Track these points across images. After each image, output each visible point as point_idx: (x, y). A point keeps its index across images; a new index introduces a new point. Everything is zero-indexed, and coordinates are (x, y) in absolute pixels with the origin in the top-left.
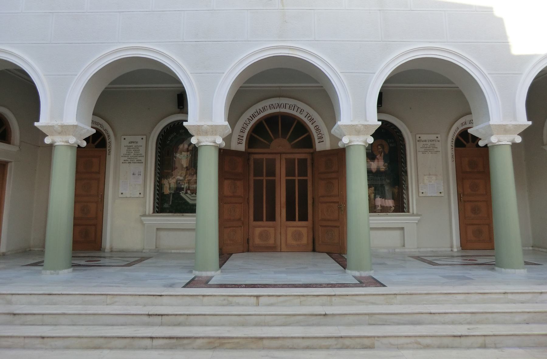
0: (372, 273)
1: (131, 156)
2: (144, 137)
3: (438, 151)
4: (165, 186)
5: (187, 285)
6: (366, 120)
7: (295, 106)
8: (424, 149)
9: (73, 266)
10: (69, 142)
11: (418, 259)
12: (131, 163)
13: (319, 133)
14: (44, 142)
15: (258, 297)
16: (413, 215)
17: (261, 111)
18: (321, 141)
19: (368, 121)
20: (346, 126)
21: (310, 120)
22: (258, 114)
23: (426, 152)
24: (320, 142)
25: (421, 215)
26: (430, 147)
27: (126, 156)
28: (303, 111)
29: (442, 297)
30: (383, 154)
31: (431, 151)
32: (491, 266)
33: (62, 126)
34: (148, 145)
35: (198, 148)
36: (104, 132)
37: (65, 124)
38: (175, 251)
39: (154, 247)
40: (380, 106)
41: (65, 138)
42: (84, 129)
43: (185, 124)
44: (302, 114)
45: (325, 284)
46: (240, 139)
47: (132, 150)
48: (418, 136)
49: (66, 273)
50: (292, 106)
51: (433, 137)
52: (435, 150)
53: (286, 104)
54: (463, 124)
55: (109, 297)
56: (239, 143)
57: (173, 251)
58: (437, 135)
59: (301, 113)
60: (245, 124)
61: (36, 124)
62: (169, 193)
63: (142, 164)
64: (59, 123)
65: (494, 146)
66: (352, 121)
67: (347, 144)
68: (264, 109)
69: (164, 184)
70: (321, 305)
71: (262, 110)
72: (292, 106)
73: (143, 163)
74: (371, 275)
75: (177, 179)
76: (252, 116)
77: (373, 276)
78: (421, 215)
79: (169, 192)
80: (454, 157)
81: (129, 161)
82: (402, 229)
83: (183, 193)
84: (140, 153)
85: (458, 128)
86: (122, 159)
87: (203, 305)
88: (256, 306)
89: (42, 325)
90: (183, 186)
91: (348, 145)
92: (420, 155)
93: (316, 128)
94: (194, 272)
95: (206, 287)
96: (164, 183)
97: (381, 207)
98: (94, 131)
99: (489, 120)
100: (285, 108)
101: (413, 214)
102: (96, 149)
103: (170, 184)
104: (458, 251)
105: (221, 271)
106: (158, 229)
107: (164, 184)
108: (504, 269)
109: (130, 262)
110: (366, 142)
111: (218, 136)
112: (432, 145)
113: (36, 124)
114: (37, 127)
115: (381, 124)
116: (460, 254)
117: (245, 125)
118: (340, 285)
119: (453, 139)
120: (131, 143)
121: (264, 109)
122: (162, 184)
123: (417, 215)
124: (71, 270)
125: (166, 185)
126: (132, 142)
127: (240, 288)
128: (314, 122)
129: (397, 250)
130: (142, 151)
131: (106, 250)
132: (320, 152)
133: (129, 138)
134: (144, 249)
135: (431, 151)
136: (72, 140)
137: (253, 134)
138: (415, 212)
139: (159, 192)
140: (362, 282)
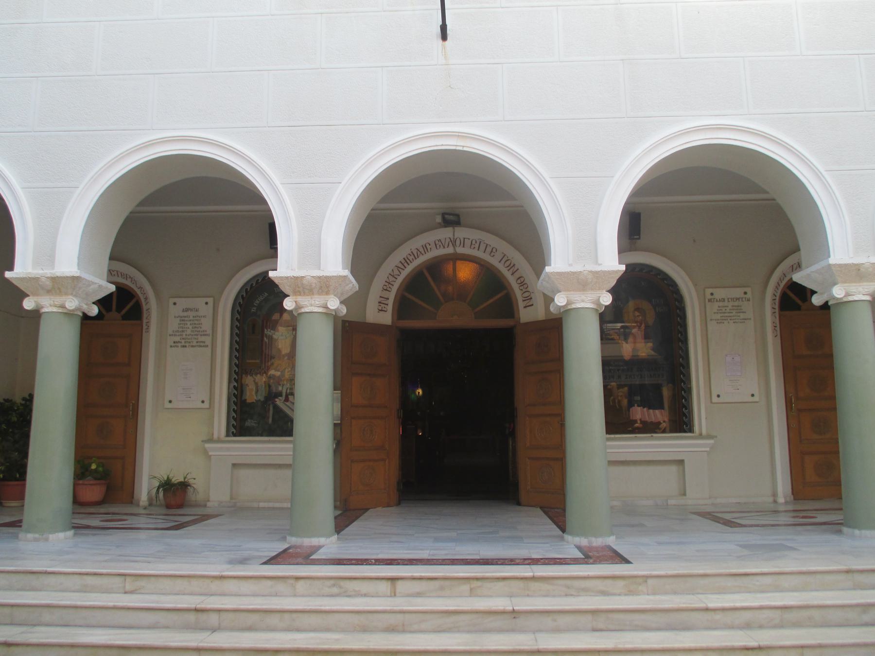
0: (611, 541)
1: (186, 335)
2: (210, 301)
3: (748, 319)
4: (248, 388)
5: (272, 561)
6: (596, 262)
7: (480, 242)
8: (722, 315)
9: (74, 528)
10: (65, 308)
11: (708, 516)
12: (186, 346)
13: (524, 290)
14: (22, 307)
15: (393, 580)
16: (701, 436)
17: (420, 252)
18: (528, 305)
19: (601, 264)
20: (561, 275)
21: (509, 268)
22: (414, 258)
23: (724, 321)
24: (528, 306)
25: (716, 437)
26: (731, 311)
27: (178, 334)
28: (496, 251)
29: (730, 582)
30: (643, 325)
31: (734, 318)
32: (836, 527)
33: (55, 279)
34: (217, 316)
35: (296, 317)
36: (138, 292)
37: (59, 274)
38: (266, 505)
39: (227, 498)
40: (636, 239)
41: (58, 300)
42: (93, 283)
43: (272, 274)
44: (494, 256)
45: (521, 559)
46: (382, 302)
47: (189, 323)
48: (709, 291)
49: (62, 538)
50: (476, 242)
51: (738, 293)
52: (742, 316)
53: (464, 238)
54: (795, 267)
55: (128, 579)
56: (380, 310)
57: (262, 505)
58: (746, 290)
59: (492, 254)
60: (390, 277)
61: (8, 274)
62: (255, 401)
63: (205, 348)
64: (48, 272)
65: (841, 304)
66: (570, 265)
67: (563, 306)
68: (426, 250)
69: (247, 385)
70: (508, 596)
71: (421, 250)
72: (476, 242)
73: (207, 346)
74: (611, 545)
75: (271, 374)
76: (403, 261)
77: (612, 546)
78: (716, 437)
79: (255, 398)
80: (778, 329)
81: (183, 344)
82: (681, 462)
83: (280, 400)
84: (202, 329)
85: (784, 275)
86: (170, 341)
87: (295, 596)
88: (391, 596)
89: (11, 624)
90: (280, 388)
91: (564, 310)
92: (712, 326)
93: (519, 281)
94: (288, 538)
95: (304, 563)
96: (246, 383)
97: (641, 423)
98: (112, 288)
99: (829, 256)
100: (464, 247)
101: (701, 434)
102: (125, 322)
103: (256, 384)
104: (786, 503)
105: (338, 538)
106: (234, 465)
107: (247, 385)
108: (859, 530)
109: (177, 523)
110: (598, 302)
111: (332, 296)
112: (736, 308)
113: (8, 274)
114: (10, 280)
115: (625, 269)
116: (790, 508)
117: (391, 279)
118: (546, 561)
119: (776, 296)
120: (186, 311)
121: (426, 250)
122: (242, 385)
123: (709, 437)
124: (70, 533)
125: (250, 387)
126: (186, 310)
127: (365, 565)
128: (516, 271)
129: (671, 502)
130: (206, 324)
131: (141, 503)
132: (527, 324)
133: (183, 303)
134: (209, 501)
135: (734, 318)
136: (72, 303)
137: (407, 294)
138: (704, 432)
139: (237, 399)
140: (588, 557)
